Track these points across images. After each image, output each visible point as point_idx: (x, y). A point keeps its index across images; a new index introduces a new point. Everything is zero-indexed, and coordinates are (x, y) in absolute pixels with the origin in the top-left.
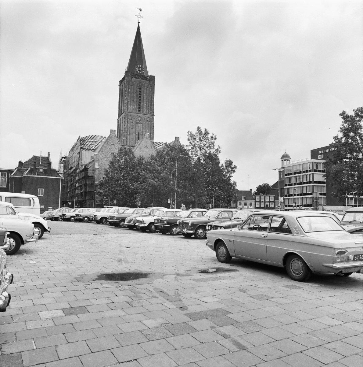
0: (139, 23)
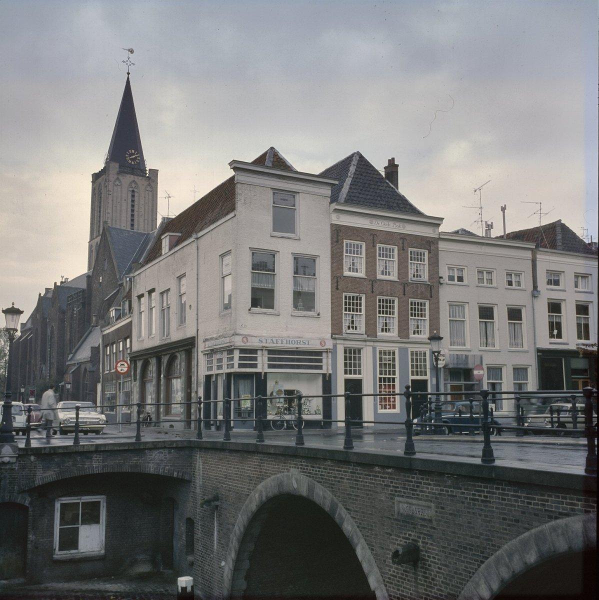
0: (128, 74)
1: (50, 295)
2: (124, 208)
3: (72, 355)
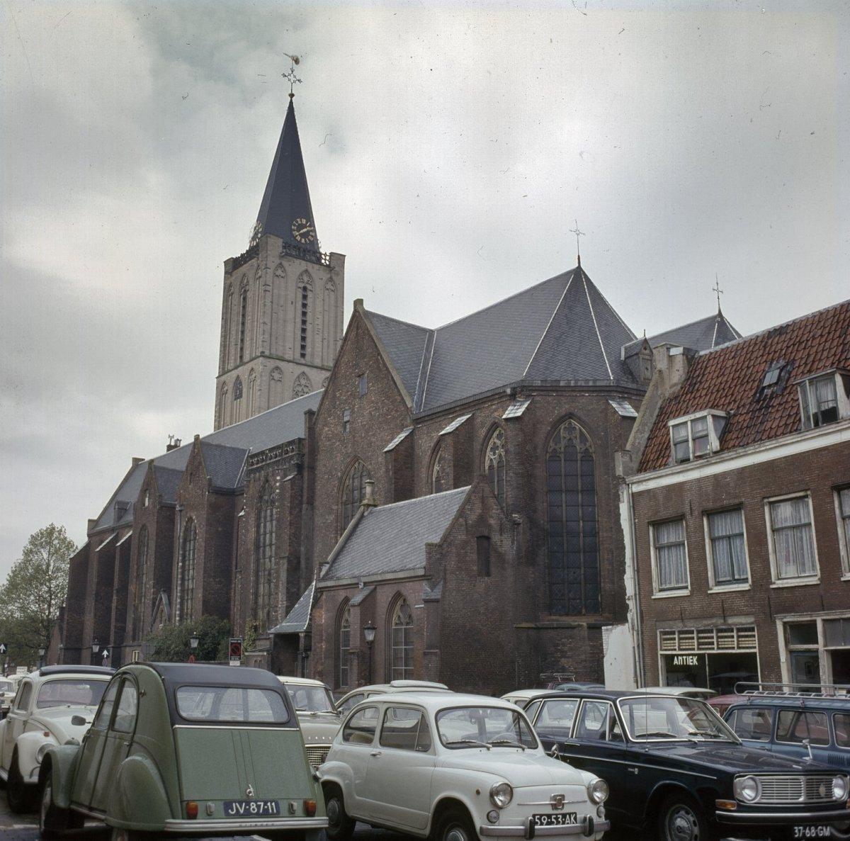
0: (292, 95)
1: (182, 465)
2: (290, 315)
3: (328, 566)
